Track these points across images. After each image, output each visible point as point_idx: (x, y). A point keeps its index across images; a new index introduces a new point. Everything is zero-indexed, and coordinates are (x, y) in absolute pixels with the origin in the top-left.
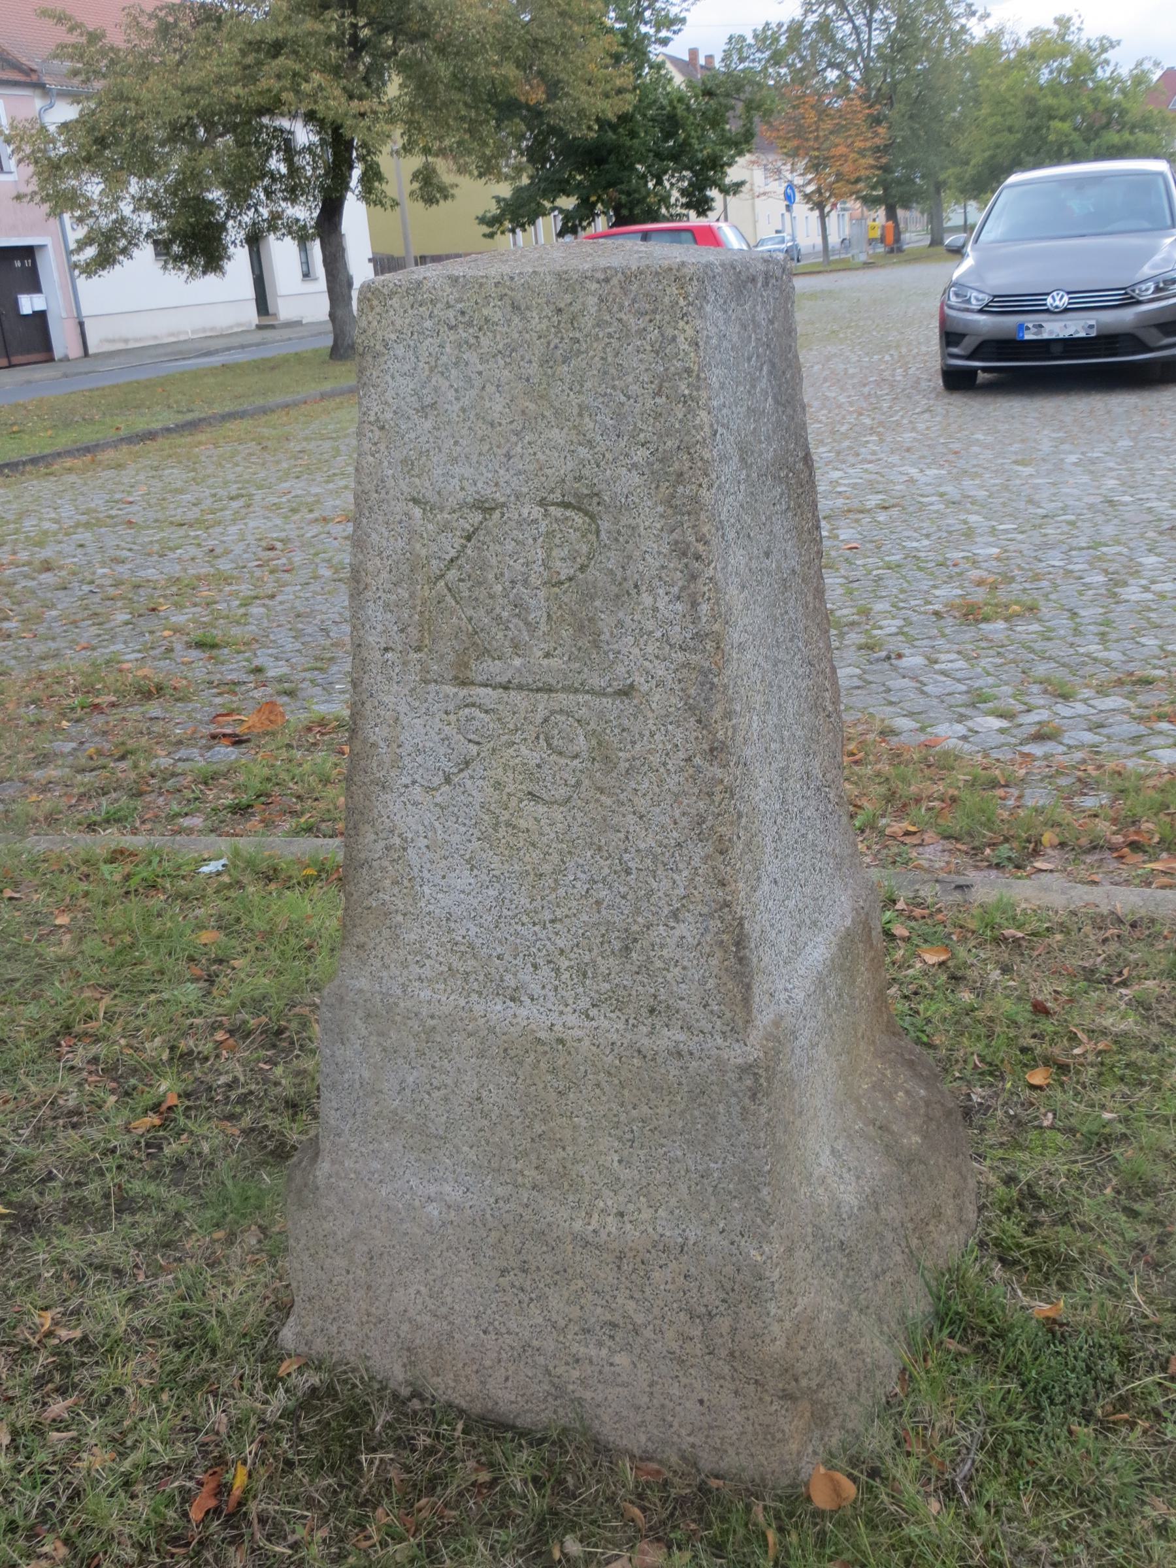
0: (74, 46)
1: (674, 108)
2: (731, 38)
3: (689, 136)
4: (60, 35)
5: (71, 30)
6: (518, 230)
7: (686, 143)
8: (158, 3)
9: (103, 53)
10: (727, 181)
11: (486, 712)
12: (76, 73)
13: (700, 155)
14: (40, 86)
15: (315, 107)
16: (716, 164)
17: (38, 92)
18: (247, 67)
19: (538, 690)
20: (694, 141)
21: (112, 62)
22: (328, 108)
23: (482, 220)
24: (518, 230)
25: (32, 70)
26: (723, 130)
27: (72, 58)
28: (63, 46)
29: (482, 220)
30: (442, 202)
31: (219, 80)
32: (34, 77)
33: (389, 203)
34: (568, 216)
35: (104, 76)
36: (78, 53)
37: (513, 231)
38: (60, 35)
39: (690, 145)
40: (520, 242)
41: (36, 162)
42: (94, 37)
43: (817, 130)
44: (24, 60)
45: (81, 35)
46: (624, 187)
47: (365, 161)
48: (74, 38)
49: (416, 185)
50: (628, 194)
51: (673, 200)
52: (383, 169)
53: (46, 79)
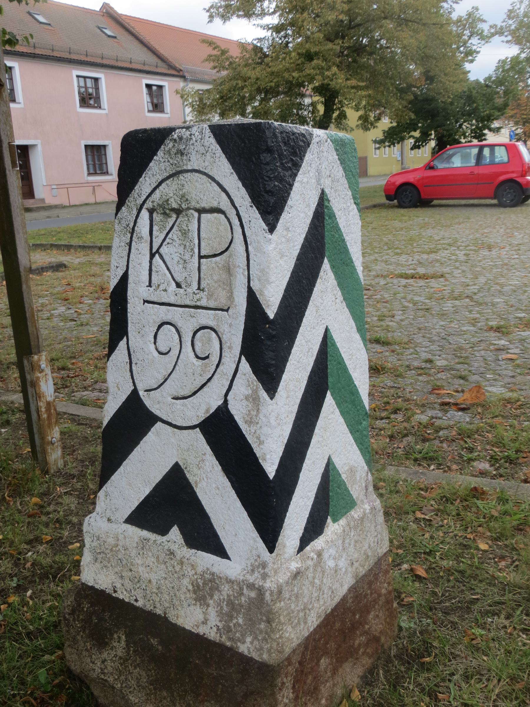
0: (215, 56)
1: (471, 92)
2: (499, 61)
3: (478, 105)
4: (210, 51)
5: (214, 49)
6: (392, 146)
7: (477, 109)
8: (255, 38)
9: (227, 59)
10: (493, 126)
11: (463, 410)
12: (215, 68)
13: (482, 114)
14: (183, 77)
15: (331, 83)
16: (489, 118)
17: (182, 79)
18: (298, 65)
19: (92, 247)
20: (480, 107)
21: (231, 63)
22: (337, 83)
23: (375, 142)
24: (392, 146)
25: (181, 70)
26: (494, 103)
27: (214, 61)
28: (210, 56)
29: (375, 142)
30: (372, 130)
31: (287, 70)
32: (181, 73)
33: (349, 129)
34: (417, 140)
35: (227, 69)
36: (216, 59)
37: (389, 146)
38: (210, 51)
39: (479, 109)
40: (387, 152)
41: (193, 106)
42: (224, 52)
43: (526, 106)
44: (177, 66)
45: (219, 51)
46: (445, 128)
47: (340, 110)
48: (216, 52)
49: (360, 122)
50: (447, 131)
51: (467, 134)
52: (347, 114)
53: (186, 74)
